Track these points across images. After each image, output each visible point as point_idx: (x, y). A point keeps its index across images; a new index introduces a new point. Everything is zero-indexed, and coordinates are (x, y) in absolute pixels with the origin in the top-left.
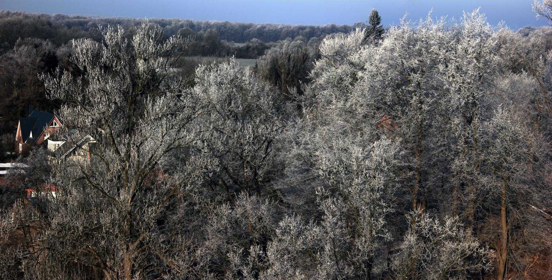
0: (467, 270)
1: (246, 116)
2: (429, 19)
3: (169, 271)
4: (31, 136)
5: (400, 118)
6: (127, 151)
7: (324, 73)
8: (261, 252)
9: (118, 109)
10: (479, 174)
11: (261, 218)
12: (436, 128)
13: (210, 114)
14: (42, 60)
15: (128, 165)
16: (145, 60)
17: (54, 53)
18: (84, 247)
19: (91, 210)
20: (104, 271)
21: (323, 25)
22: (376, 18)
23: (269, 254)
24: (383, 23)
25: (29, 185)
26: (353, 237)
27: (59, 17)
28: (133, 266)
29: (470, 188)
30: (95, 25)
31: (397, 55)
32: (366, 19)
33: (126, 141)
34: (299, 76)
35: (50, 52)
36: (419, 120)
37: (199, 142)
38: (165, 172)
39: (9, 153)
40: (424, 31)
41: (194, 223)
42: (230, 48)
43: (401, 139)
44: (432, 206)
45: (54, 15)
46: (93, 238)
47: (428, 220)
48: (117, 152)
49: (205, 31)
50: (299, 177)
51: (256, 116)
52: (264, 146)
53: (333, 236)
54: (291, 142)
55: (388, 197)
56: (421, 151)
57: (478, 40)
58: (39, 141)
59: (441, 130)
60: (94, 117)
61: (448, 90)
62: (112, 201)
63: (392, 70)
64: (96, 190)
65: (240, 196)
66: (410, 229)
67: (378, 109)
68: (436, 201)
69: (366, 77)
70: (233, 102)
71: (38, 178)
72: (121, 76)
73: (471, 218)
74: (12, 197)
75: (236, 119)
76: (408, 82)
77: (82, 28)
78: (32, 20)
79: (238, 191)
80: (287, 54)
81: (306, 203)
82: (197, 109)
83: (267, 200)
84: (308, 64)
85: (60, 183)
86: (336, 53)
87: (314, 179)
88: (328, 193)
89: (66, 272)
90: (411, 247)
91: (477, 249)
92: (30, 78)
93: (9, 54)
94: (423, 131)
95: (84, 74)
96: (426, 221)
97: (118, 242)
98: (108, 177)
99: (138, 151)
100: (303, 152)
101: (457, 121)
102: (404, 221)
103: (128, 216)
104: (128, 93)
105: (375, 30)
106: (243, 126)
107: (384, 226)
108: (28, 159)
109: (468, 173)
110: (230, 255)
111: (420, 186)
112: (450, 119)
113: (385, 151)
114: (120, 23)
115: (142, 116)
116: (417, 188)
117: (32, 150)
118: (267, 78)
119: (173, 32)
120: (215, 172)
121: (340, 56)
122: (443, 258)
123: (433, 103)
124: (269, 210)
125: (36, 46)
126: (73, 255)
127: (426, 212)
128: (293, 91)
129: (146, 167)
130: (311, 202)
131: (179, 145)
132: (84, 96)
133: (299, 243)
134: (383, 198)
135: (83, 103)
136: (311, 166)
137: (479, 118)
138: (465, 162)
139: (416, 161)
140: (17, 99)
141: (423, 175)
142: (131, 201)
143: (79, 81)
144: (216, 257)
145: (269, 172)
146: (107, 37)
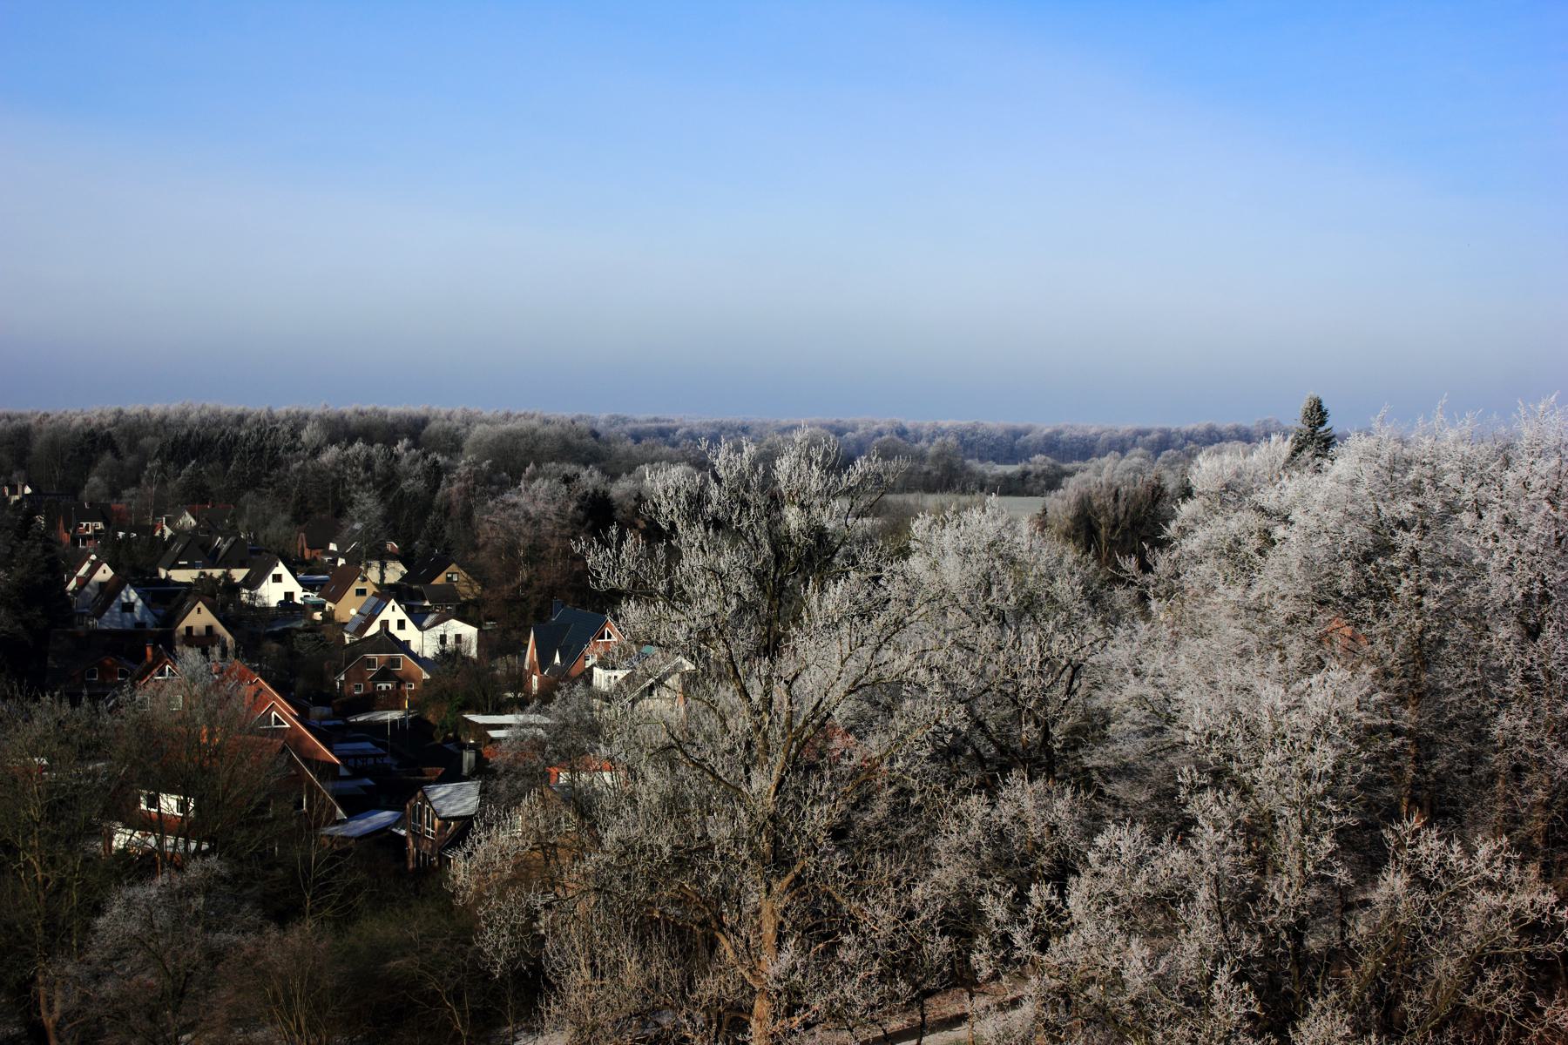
0: (1528, 954)
1: (1023, 615)
2: (1439, 417)
3: (855, 927)
4: (557, 660)
5: (1371, 624)
6: (766, 693)
7: (1197, 528)
8: (1054, 898)
9: (744, 608)
10: (1556, 747)
11: (1056, 827)
12: (1455, 646)
13: (945, 614)
14: (580, 507)
15: (767, 719)
16: (802, 506)
17: (605, 493)
18: (675, 887)
19: (688, 812)
20: (718, 934)
21: (1195, 423)
22: (1317, 413)
23: (1071, 902)
24: (1334, 424)
25: (555, 759)
26: (1263, 873)
27: (616, 420)
28: (781, 924)
29: (1534, 778)
30: (693, 436)
31: (1365, 492)
32: (1296, 421)
33: (764, 672)
34: (1143, 532)
35: (596, 491)
36: (1417, 630)
37: (922, 672)
38: (849, 730)
39: (510, 695)
40: (1427, 442)
41: (909, 831)
42: (985, 476)
43: (1373, 669)
44: (1444, 810)
45: (604, 416)
46: (693, 868)
47: (1436, 845)
48: (744, 693)
49: (930, 442)
50: (1141, 744)
51: (1045, 616)
52: (1065, 677)
53: (1214, 871)
54: (1124, 670)
55: (1344, 789)
56: (1420, 695)
57: (1554, 462)
58: (575, 671)
59: (1465, 650)
60: (692, 624)
61: (1483, 567)
62: (733, 793)
63: (1352, 524)
64: (698, 771)
65: (1010, 780)
66: (1392, 863)
67: (1322, 603)
68: (1456, 803)
69: (1293, 539)
70: (994, 588)
71: (574, 746)
72: (750, 539)
73: (1536, 841)
74: (519, 784)
75: (1002, 619)
76: (1388, 549)
77: (662, 442)
78: (558, 427)
79: (1005, 769)
80: (1110, 486)
81: (1156, 798)
82: (916, 604)
83: (1068, 790)
84: (1164, 506)
85: (621, 757)
86: (1227, 486)
87: (1174, 748)
88: (1206, 779)
89: (634, 937)
90: (1394, 900)
91: (1552, 910)
92: (555, 543)
93: (510, 497)
94: (1423, 653)
95: (669, 538)
96: (1430, 845)
97: (748, 877)
98: (726, 745)
99: (788, 691)
100: (1151, 692)
101: (1503, 633)
102: (1380, 843)
103: (770, 825)
104: (765, 574)
105: (1316, 438)
106: (1019, 638)
107: (1331, 854)
108: (552, 707)
109: (1530, 744)
110: (987, 901)
111: (1417, 772)
112: (1487, 629)
113: (1337, 695)
114: (745, 430)
115: (797, 619)
116: (1410, 772)
117: (559, 689)
118: (1069, 536)
119: (861, 448)
120: (956, 732)
121: (1232, 493)
122: (1468, 926)
123: (1448, 593)
124: (1072, 811)
125: (567, 480)
126: (651, 904)
127: (1431, 827)
128: (1130, 564)
129: (806, 723)
130: (1167, 795)
131: (880, 677)
132: (670, 583)
133: (1138, 882)
134: (1330, 793)
135: (669, 595)
136: (1167, 722)
137: (1556, 628)
138: (1525, 721)
139: (1407, 717)
140: (527, 585)
141: (1425, 747)
142: (776, 793)
143: (661, 554)
144: (955, 903)
145: (1075, 730)
146: (720, 463)
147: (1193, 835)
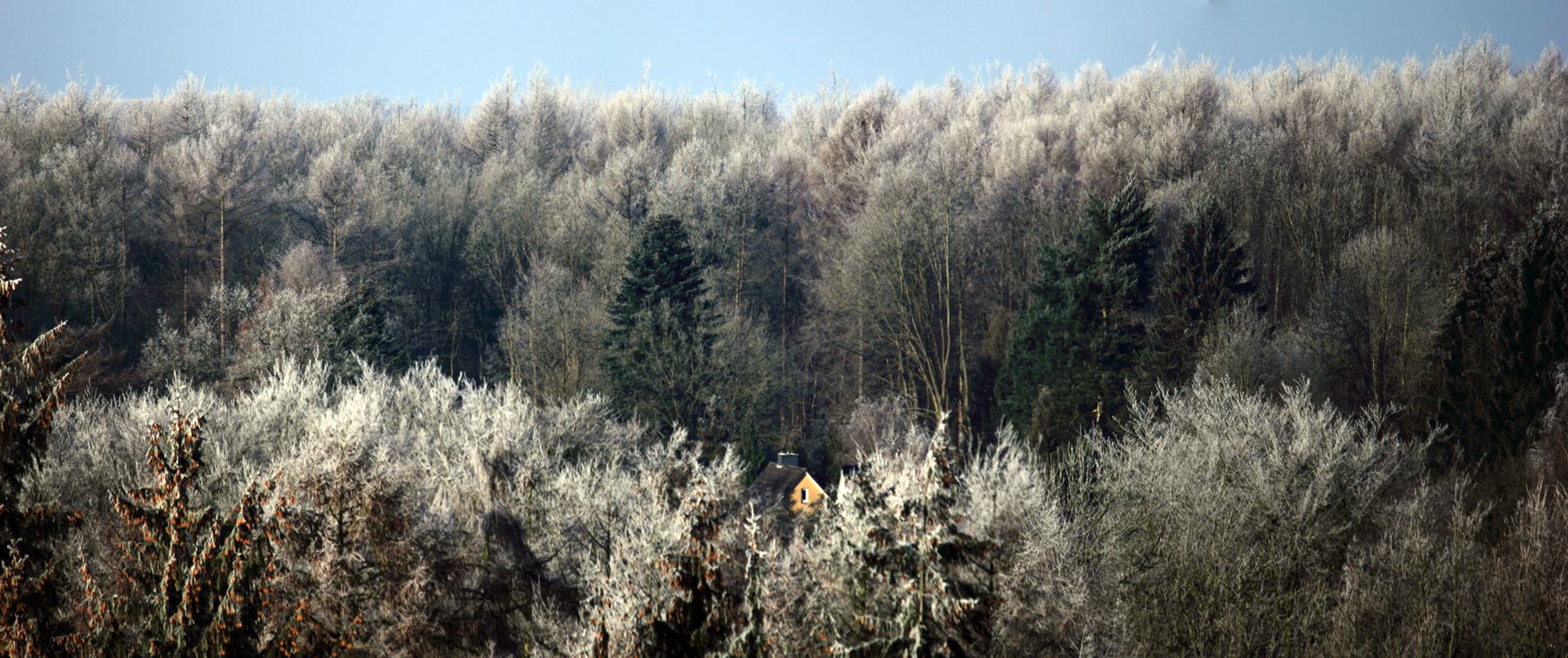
147: (66, 628)
